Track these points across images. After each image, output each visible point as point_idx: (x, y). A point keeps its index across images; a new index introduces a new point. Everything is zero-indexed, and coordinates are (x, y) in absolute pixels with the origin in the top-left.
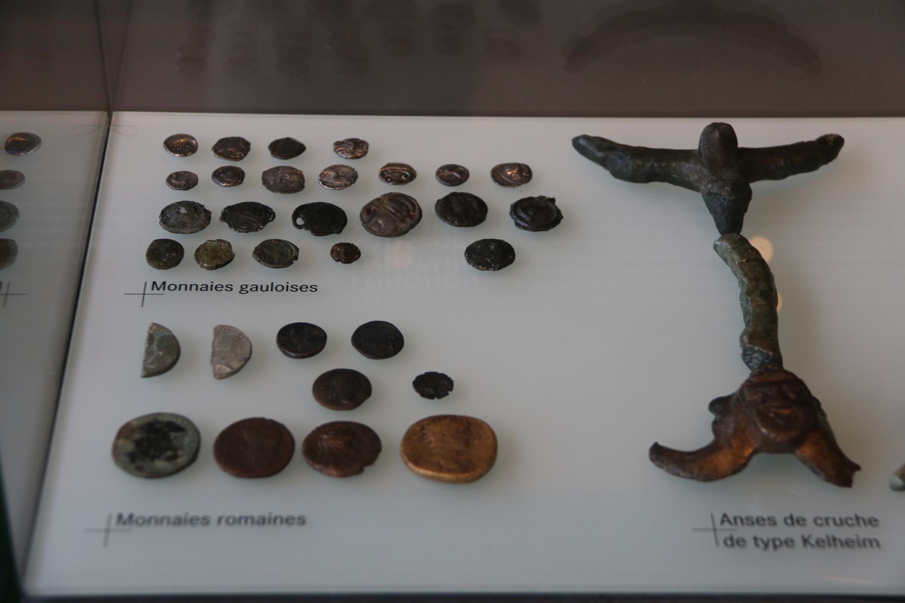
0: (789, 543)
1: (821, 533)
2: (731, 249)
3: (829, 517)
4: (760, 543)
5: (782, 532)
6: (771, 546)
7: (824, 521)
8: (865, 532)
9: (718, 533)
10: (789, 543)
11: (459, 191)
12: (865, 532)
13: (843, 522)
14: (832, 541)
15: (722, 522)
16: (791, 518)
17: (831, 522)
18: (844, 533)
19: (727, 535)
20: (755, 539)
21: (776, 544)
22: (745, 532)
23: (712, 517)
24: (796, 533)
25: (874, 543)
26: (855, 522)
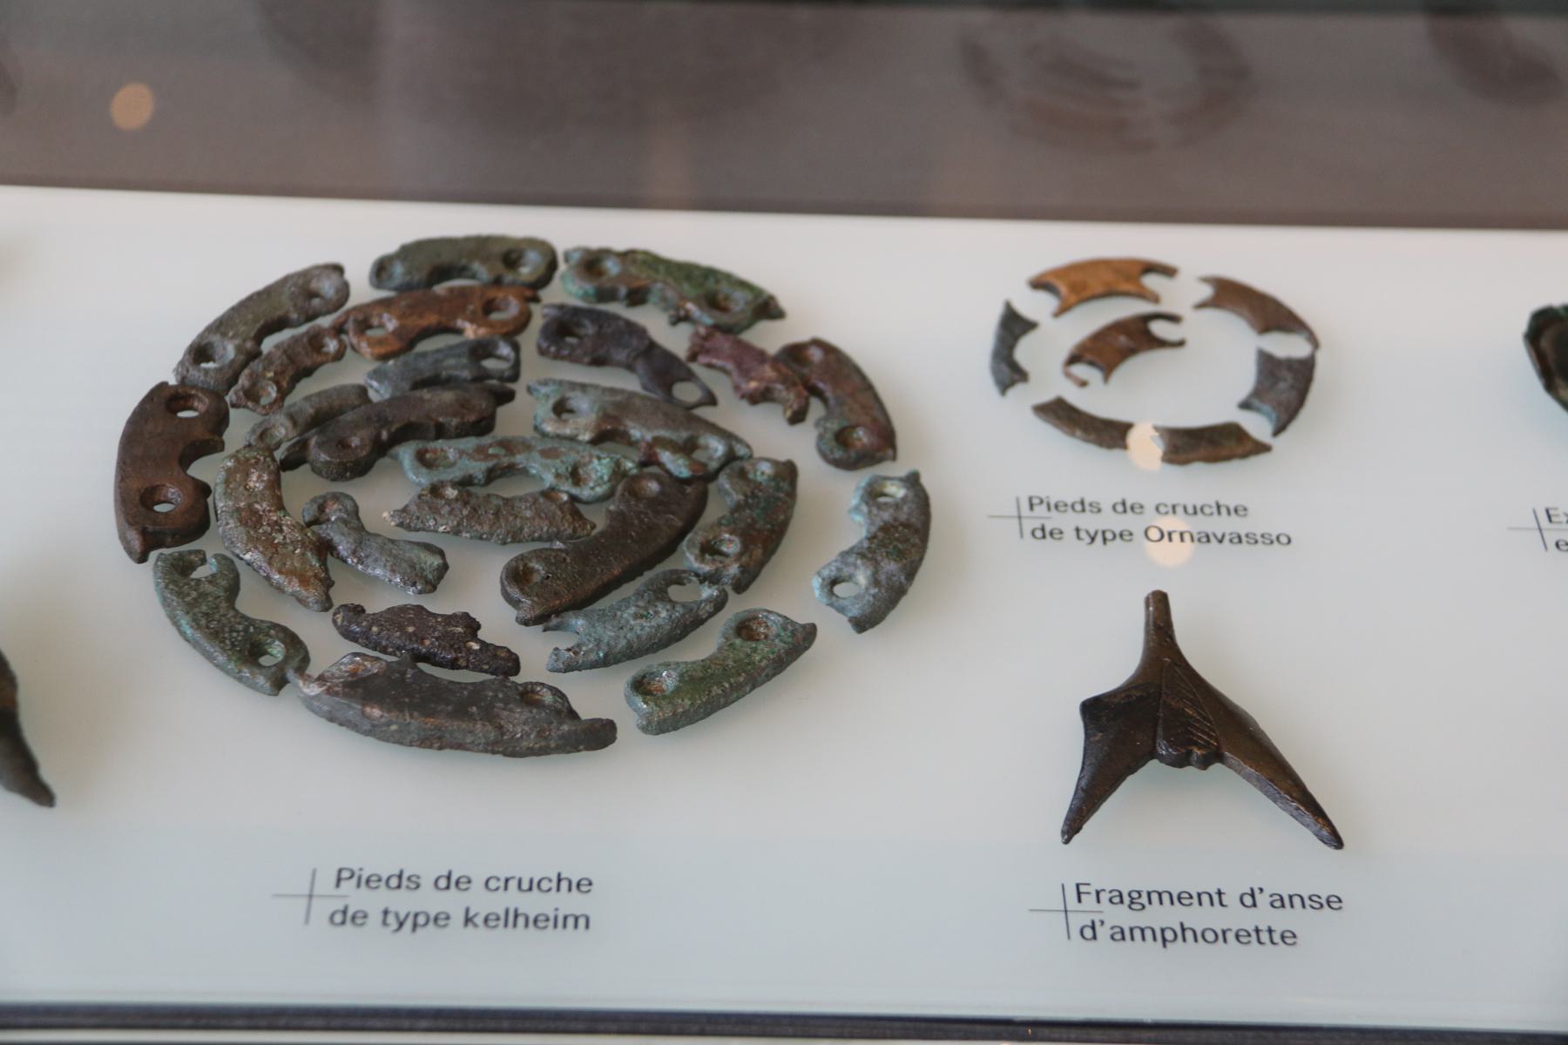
0: (440, 920)
1: (499, 903)
2: (236, 666)
3: (1178, 504)
4: (1083, 534)
5: (429, 900)
6: (1099, 538)
7: (1170, 509)
8: (569, 903)
9: (1024, 521)
10: (440, 920)
11: (192, 548)
12: (569, 903)
13: (534, 885)
14: (513, 918)
15: (1031, 506)
16: (1124, 504)
17: (1180, 510)
18: (532, 904)
19: (1037, 524)
20: (1078, 530)
21: (416, 922)
22: (372, 901)
23: (1018, 501)
24: (453, 903)
25: (581, 921)
26: (1215, 510)
